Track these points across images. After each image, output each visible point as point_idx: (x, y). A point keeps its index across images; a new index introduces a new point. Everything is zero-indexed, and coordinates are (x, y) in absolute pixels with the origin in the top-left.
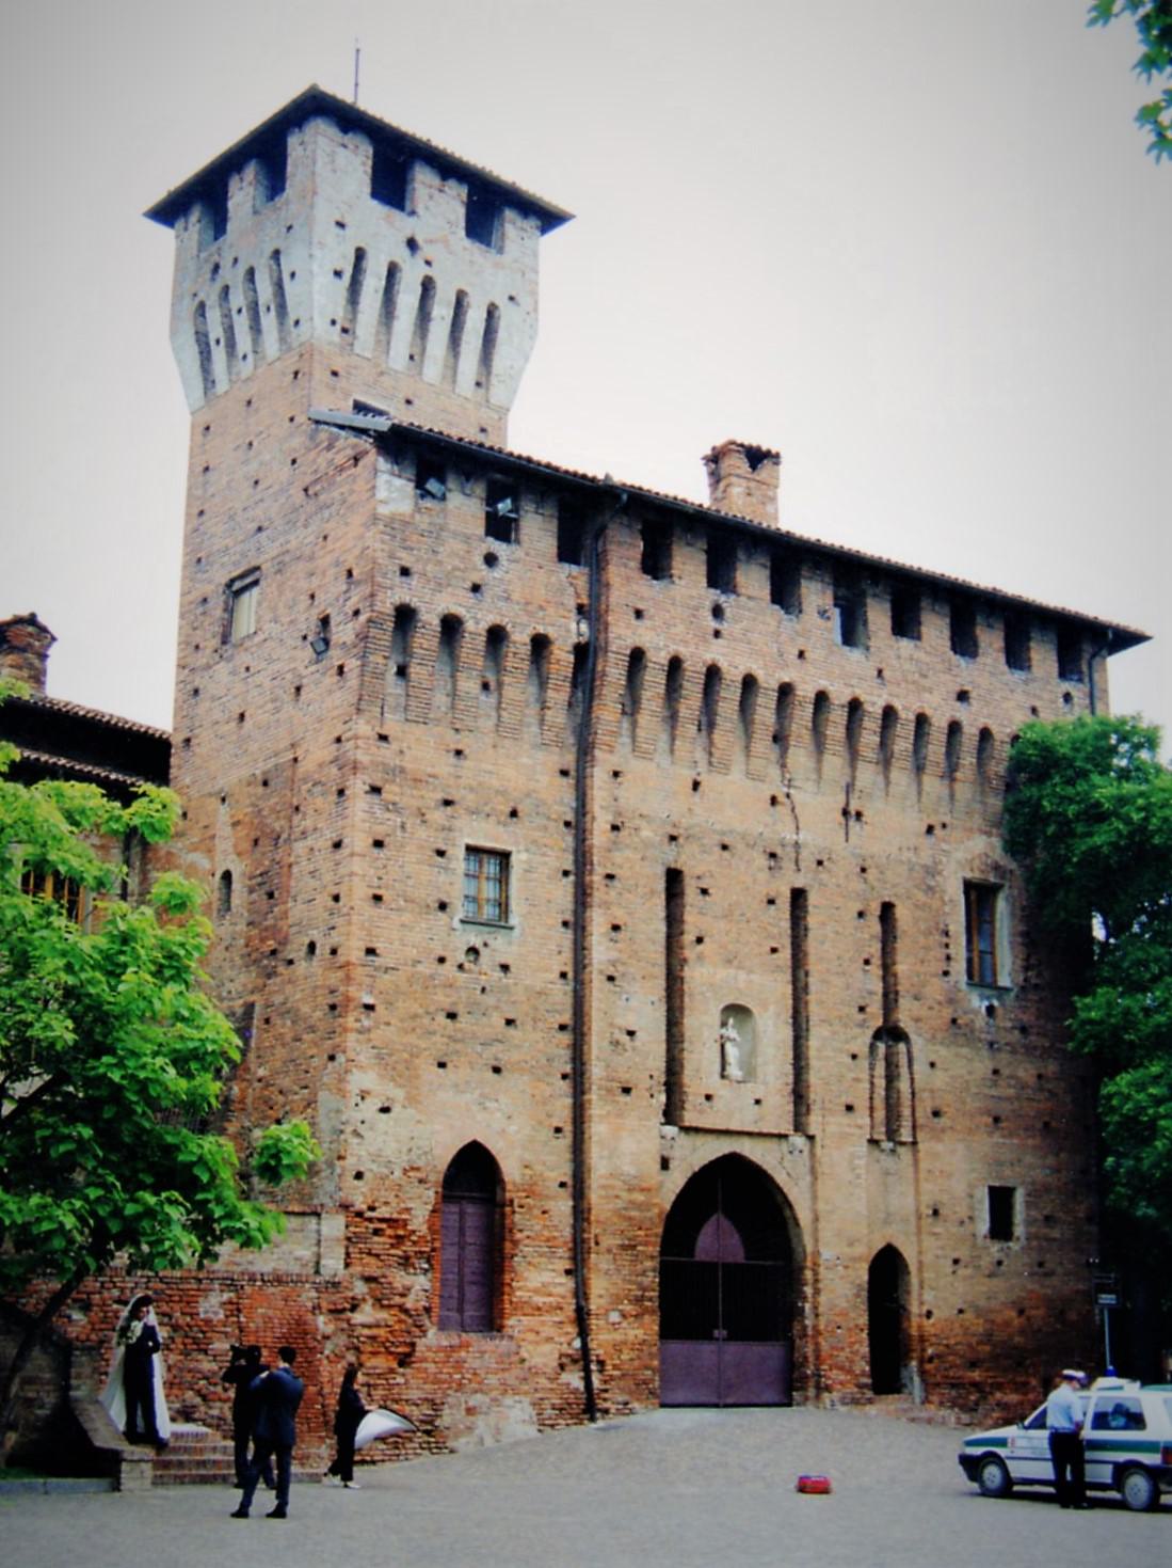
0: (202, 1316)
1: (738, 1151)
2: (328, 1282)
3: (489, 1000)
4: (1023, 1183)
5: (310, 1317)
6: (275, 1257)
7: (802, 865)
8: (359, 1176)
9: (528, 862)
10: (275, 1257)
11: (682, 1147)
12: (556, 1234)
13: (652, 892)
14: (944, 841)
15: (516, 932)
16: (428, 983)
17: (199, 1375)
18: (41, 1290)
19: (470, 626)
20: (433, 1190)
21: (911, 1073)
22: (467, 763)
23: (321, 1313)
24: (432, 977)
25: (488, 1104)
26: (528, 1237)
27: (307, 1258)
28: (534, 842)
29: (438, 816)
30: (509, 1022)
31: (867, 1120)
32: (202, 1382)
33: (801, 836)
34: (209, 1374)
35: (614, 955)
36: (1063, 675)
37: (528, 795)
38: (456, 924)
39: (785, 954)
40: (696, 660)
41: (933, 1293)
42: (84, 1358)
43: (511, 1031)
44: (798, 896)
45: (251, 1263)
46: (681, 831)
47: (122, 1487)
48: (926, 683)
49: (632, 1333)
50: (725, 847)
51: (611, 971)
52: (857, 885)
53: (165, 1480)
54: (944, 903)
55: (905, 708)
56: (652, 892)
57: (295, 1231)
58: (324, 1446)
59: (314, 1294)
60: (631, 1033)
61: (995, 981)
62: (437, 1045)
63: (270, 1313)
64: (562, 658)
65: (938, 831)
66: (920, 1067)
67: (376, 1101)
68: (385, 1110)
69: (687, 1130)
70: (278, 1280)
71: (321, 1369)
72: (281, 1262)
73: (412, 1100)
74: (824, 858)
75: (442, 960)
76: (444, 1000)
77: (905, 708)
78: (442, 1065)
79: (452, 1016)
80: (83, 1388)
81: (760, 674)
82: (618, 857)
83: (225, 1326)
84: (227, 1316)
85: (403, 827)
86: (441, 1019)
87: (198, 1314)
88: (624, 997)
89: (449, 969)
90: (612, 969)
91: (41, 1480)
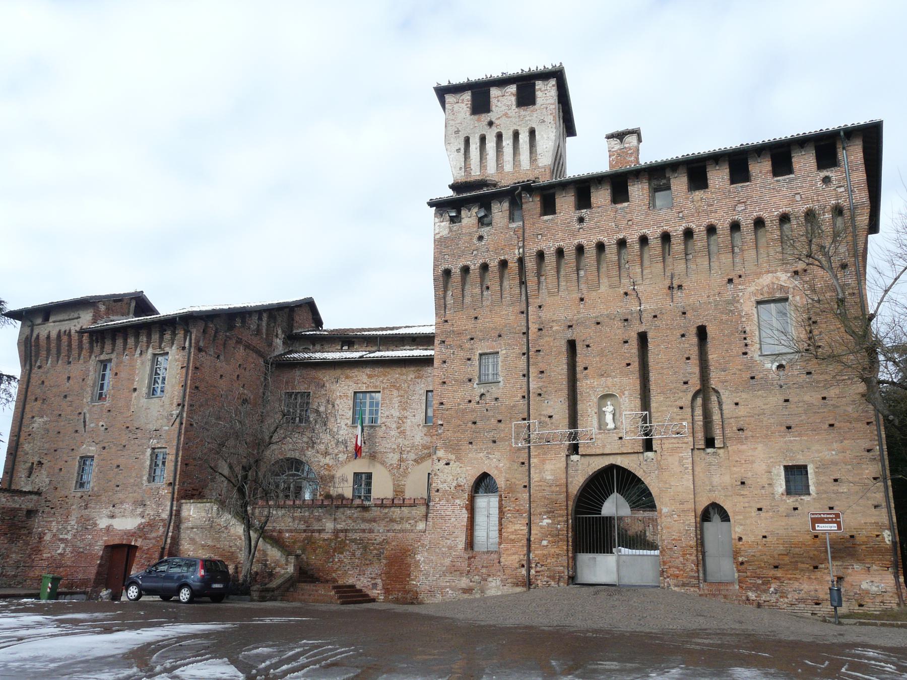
1: (614, 463)
3: (490, 413)
4: (813, 462)
7: (644, 320)
8: (438, 491)
9: (506, 353)
11: (582, 464)
12: (522, 508)
13: (560, 353)
14: (740, 284)
15: (501, 384)
16: (464, 411)
19: (472, 267)
20: (467, 494)
21: (721, 410)
22: (479, 321)
24: (466, 408)
25: (490, 456)
26: (509, 510)
28: (509, 344)
29: (468, 345)
30: (500, 421)
31: (691, 439)
33: (642, 307)
35: (541, 384)
36: (821, 166)
37: (505, 326)
38: (475, 386)
39: (635, 365)
40: (569, 246)
41: (742, 527)
43: (500, 424)
44: (643, 338)
46: (574, 322)
48: (713, 208)
49: (553, 550)
50: (598, 323)
51: (539, 391)
52: (681, 321)
54: (742, 317)
55: (697, 226)
56: (560, 353)
60: (550, 417)
62: (468, 435)
64: (513, 265)
65: (736, 281)
66: (728, 407)
67: (444, 461)
68: (447, 464)
69: (582, 455)
73: (458, 459)
74: (657, 313)
75: (470, 401)
76: (471, 417)
77: (697, 226)
78: (471, 443)
79: (474, 423)
81: (605, 240)
82: (542, 342)
85: (453, 353)
86: (470, 424)
88: (546, 401)
89: (473, 405)
90: (540, 390)
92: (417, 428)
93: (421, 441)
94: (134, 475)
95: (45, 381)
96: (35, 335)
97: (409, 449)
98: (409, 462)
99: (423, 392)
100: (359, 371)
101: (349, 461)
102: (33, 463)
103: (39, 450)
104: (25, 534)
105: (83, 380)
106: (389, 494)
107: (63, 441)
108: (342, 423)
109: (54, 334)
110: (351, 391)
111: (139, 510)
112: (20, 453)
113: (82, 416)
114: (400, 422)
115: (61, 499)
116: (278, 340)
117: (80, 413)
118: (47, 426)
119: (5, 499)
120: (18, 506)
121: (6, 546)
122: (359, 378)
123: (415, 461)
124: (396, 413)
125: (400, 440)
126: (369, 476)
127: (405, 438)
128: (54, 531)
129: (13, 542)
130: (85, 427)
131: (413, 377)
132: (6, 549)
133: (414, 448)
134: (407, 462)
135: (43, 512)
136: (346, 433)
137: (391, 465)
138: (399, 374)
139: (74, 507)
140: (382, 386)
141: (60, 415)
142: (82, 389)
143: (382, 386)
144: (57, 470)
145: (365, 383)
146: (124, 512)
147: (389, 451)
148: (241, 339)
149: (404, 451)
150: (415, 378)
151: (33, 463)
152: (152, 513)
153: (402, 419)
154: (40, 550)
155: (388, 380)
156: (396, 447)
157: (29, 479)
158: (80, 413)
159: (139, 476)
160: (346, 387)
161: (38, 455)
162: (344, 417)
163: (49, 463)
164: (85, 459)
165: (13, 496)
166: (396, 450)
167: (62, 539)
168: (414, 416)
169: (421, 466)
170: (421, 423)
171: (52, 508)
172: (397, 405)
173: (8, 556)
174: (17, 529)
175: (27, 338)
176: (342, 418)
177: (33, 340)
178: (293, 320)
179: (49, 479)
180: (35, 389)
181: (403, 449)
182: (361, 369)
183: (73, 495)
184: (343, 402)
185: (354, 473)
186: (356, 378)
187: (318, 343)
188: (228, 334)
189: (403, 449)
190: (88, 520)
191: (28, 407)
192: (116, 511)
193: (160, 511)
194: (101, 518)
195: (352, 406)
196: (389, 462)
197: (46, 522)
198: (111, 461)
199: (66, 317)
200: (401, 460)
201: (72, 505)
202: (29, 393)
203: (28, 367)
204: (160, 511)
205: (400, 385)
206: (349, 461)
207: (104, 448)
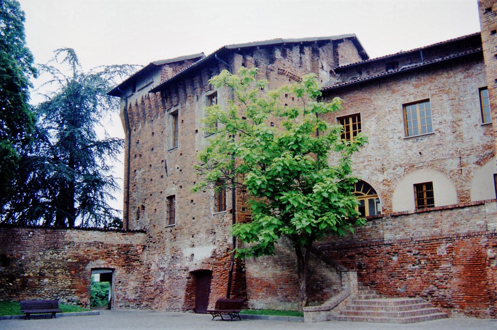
0: (438, 254)
2: (492, 233)
5: (484, 249)
6: (468, 225)
10: (468, 225)
17: (435, 278)
18: (384, 251)
23: (489, 248)
27: (482, 224)
32: (436, 281)
34: (439, 278)
42: (345, 275)
45: (458, 230)
47: (305, 321)
53: (348, 319)
57: (476, 213)
58: (488, 309)
59: (486, 239)
61: (364, 56)
63: (466, 250)
70: (469, 235)
71: (488, 273)
72: (471, 227)
80: (346, 285)
83: (446, 258)
84: (448, 253)
87: (436, 254)
91: (288, 317)
92: (474, 129)
93: (481, 141)
94: (204, 207)
95: (139, 140)
96: (128, 106)
97: (468, 152)
98: (470, 166)
99: (476, 90)
100: (404, 83)
101: (407, 173)
102: (139, 208)
103: (141, 196)
104: (138, 265)
105: (162, 132)
106: (453, 201)
107: (154, 186)
108: (395, 137)
109: (139, 102)
110: (399, 105)
111: (212, 237)
112: (131, 201)
113: (164, 163)
114: (455, 125)
115: (158, 235)
116: (324, 72)
117: (163, 161)
118: (144, 176)
119: (118, 238)
120: (129, 243)
121: (125, 275)
122: (405, 91)
123: (478, 163)
124: (449, 117)
125: (457, 145)
126: (429, 185)
127: (463, 142)
128: (157, 262)
129: (129, 273)
130: (167, 172)
131: (462, 77)
132: (125, 277)
133: (474, 151)
134: (468, 166)
135: (149, 246)
136: (401, 146)
137: (451, 171)
138: (446, 78)
139: (167, 240)
140: (430, 93)
141: (151, 165)
142: (162, 140)
143: (430, 93)
144: (153, 211)
145: (413, 94)
146: (201, 241)
147: (448, 157)
148: (284, 71)
149: (463, 155)
150: (464, 78)
151: (139, 208)
152: (221, 240)
153: (456, 123)
154: (149, 278)
155: (435, 86)
156: (454, 152)
157: (138, 221)
158: (163, 161)
159: (207, 207)
160: (394, 102)
161: (141, 201)
162: (396, 131)
163: (148, 206)
164: (171, 198)
165: (125, 235)
166: (455, 155)
167: (162, 268)
168: (469, 117)
169: (485, 167)
170: (478, 123)
171: (154, 243)
172: (448, 109)
173: (128, 284)
174: (131, 261)
175: (125, 110)
176: (394, 133)
177: (128, 109)
178: (338, 55)
179: (150, 219)
180: (135, 149)
181: (462, 153)
182: (406, 81)
183: (165, 230)
184: (392, 117)
185: (415, 185)
186: (403, 91)
187: (364, 71)
188: (269, 66)
189: (462, 153)
190: (177, 251)
191: (131, 163)
192: (195, 240)
193: (227, 237)
194: (185, 248)
195: (402, 119)
196: (449, 168)
197: (152, 255)
198: (186, 198)
199: (145, 85)
200: (461, 165)
201: (166, 239)
202: (131, 152)
203: (128, 133)
204: (227, 237)
205: (449, 89)
206: (407, 173)
207: (181, 187)
